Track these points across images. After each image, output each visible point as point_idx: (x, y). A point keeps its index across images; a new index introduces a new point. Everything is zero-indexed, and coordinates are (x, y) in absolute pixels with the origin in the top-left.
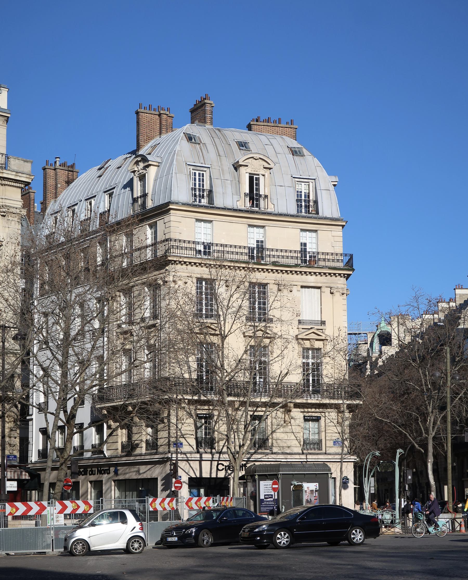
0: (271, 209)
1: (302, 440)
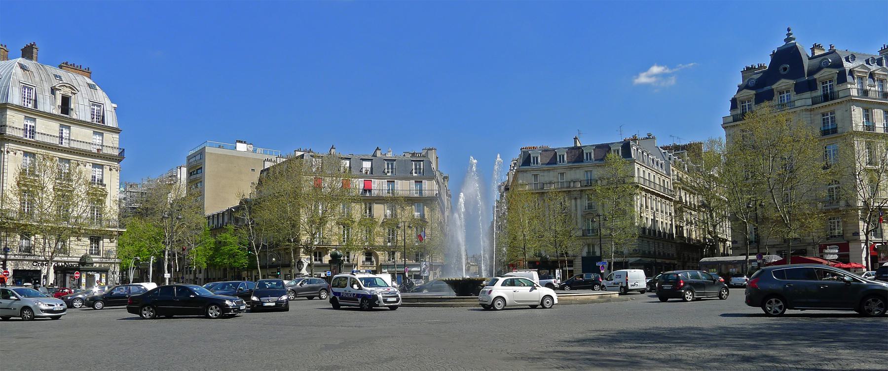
0: (75, 117)
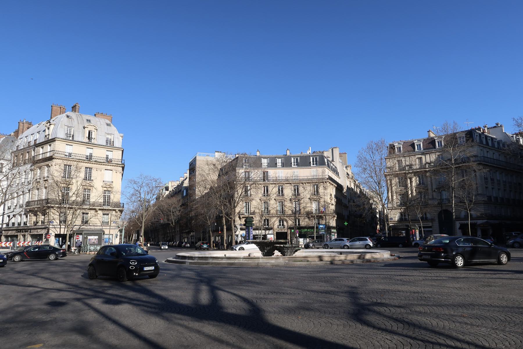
1: (101, 221)
